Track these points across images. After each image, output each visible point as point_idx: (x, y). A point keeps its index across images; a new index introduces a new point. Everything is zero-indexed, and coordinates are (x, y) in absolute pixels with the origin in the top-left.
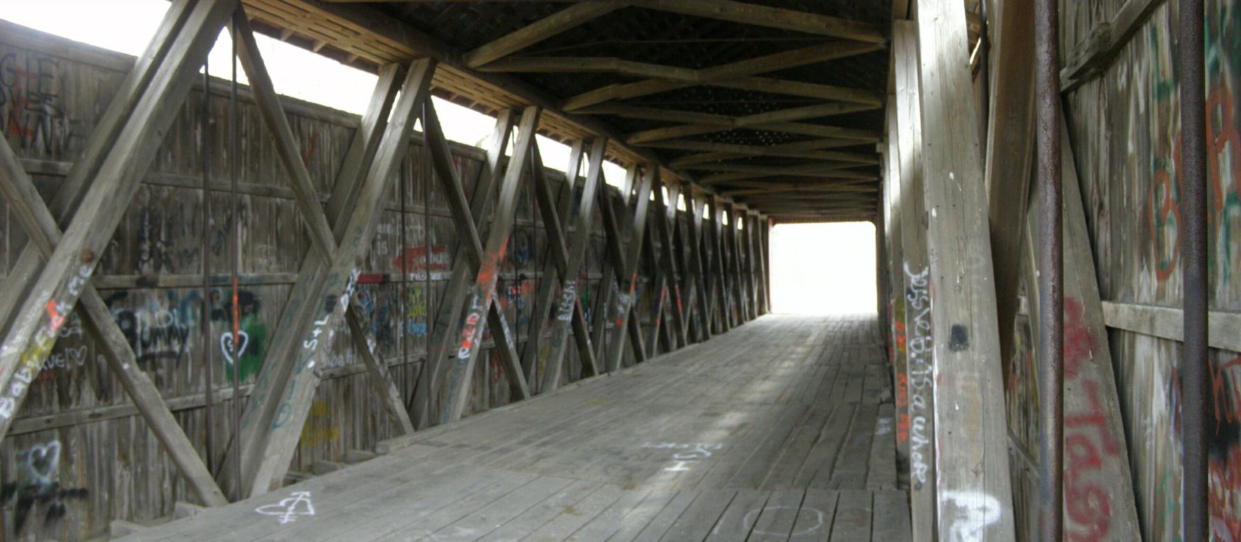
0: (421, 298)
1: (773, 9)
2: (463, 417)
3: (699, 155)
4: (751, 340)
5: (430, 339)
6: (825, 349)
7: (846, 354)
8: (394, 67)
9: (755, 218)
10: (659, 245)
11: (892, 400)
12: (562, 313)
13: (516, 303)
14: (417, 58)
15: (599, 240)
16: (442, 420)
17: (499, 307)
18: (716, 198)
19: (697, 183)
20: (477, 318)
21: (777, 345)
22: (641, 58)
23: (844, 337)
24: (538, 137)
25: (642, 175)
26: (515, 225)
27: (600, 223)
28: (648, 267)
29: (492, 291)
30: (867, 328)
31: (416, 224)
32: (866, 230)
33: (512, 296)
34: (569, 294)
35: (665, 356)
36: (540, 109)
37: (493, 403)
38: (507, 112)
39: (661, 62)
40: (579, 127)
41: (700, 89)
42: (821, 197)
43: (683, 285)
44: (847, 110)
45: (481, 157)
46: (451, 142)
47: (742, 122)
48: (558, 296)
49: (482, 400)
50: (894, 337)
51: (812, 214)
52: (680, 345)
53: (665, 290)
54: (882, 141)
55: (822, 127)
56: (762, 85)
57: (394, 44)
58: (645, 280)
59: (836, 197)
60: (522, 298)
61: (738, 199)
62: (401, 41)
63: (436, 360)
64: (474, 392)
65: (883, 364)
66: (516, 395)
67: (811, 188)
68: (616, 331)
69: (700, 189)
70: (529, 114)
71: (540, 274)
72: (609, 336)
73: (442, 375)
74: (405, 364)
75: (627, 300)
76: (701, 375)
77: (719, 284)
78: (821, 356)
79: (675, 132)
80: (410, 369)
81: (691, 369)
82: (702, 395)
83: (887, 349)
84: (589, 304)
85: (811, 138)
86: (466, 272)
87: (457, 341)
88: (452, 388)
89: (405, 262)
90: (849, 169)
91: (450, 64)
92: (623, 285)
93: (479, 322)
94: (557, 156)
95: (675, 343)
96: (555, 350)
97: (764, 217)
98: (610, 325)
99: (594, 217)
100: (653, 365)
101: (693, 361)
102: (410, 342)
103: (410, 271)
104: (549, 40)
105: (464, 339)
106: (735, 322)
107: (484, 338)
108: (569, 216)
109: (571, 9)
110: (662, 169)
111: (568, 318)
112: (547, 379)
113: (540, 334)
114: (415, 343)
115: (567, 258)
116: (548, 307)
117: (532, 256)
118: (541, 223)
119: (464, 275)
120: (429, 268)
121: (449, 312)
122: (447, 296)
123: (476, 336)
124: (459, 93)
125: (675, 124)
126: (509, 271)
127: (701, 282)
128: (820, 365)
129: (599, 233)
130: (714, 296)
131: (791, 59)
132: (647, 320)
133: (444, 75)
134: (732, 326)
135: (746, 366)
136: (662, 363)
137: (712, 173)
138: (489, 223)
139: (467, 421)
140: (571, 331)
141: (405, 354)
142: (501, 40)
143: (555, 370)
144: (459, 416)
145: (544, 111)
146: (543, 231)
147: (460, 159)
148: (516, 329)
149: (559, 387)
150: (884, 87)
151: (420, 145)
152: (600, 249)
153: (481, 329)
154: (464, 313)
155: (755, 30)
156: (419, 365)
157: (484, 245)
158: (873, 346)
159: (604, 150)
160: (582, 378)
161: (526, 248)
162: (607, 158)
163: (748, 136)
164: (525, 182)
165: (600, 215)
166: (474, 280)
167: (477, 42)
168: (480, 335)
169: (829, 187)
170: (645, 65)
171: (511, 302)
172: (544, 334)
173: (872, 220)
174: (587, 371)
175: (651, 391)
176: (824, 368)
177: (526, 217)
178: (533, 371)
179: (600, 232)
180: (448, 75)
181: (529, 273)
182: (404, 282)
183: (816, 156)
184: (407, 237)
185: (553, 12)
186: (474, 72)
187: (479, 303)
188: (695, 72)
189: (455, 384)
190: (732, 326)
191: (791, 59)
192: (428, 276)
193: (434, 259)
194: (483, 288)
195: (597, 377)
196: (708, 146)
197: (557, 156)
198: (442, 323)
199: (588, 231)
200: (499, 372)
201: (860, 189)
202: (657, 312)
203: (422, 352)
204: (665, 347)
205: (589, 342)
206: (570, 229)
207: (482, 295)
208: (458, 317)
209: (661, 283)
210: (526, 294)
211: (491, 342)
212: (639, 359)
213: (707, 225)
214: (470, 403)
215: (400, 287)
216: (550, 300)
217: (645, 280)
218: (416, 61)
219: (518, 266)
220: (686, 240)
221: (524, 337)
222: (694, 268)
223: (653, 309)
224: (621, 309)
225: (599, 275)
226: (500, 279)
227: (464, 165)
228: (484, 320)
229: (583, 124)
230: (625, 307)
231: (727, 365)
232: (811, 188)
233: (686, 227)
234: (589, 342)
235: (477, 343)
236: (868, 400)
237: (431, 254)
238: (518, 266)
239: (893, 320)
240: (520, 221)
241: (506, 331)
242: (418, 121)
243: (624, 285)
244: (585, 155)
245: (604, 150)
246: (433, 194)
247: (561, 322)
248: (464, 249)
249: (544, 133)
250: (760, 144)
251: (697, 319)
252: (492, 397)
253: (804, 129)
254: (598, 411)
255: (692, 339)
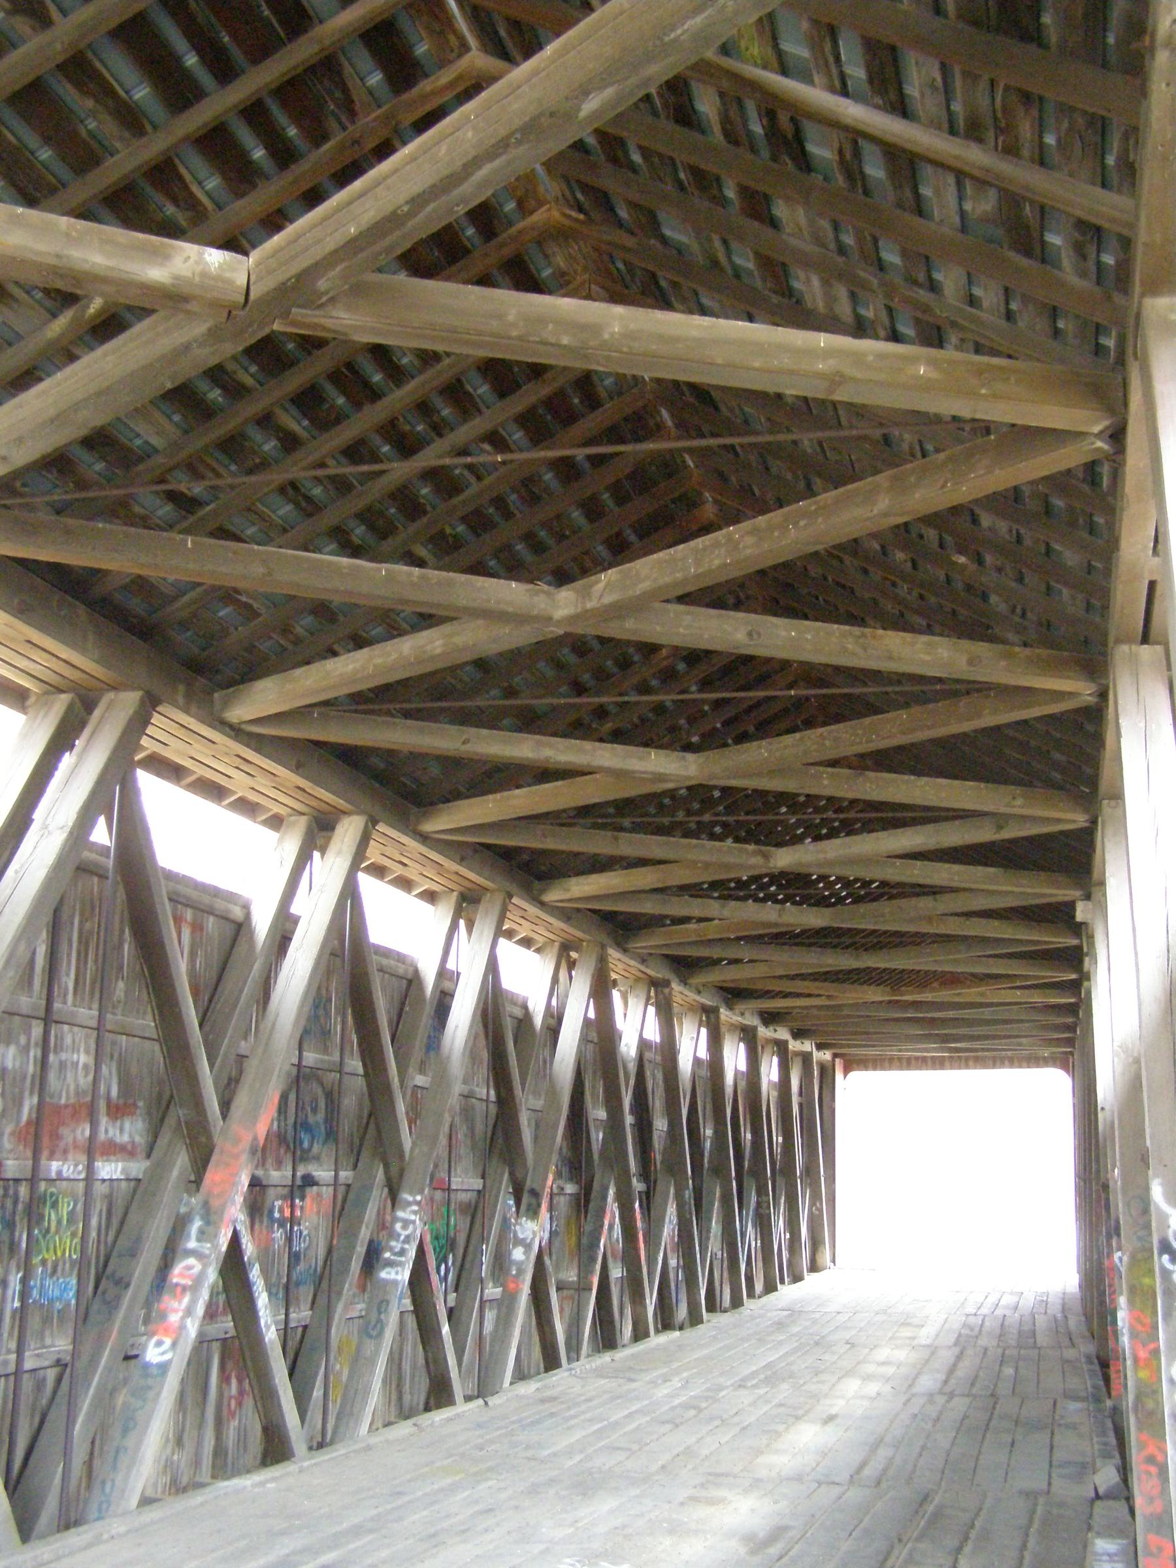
0: (72, 1214)
1: (856, 630)
2: (146, 1502)
3: (692, 926)
4: (795, 1329)
5: (84, 1317)
6: (959, 1357)
7: (1009, 1371)
8: (62, 701)
9: (806, 1058)
10: (602, 1114)
11: (1124, 1492)
12: (390, 1264)
13: (289, 1240)
14: (114, 688)
15: (480, 1107)
16: (93, 1514)
17: (249, 1247)
18: (724, 1014)
19: (684, 982)
20: (196, 1270)
21: (851, 1344)
22: (577, 729)
23: (1002, 1331)
24: (367, 883)
25: (572, 965)
26: (299, 1066)
27: (483, 1071)
28: (577, 1164)
29: (236, 1212)
30: (1055, 1309)
31: (75, 1049)
32: (1047, 1089)
33: (282, 1224)
34: (406, 1223)
35: (607, 1357)
36: (373, 821)
37: (223, 1466)
38: (303, 821)
39: (618, 736)
40: (451, 865)
41: (700, 794)
42: (951, 1014)
43: (648, 1198)
44: (1007, 834)
45: (237, 913)
46: (170, 876)
47: (784, 859)
48: (384, 1226)
49: (197, 1463)
50: (1125, 1340)
51: (933, 1050)
52: (640, 1334)
53: (612, 1207)
54: (1088, 897)
55: (956, 867)
56: (830, 784)
57: (65, 652)
58: (570, 1188)
59: (986, 1014)
60: (305, 1227)
61: (770, 1018)
62: (83, 651)
63: (94, 1361)
64: (179, 1442)
65: (1098, 1400)
66: (275, 1449)
67: (928, 996)
68: (506, 1304)
69: (692, 996)
70: (348, 831)
71: (345, 1175)
72: (490, 1316)
73: (107, 1395)
74: (18, 1372)
75: (533, 1230)
76: (686, 1406)
77: (726, 1200)
78: (951, 1371)
79: (645, 878)
80: (27, 1383)
81: (663, 1391)
82: (688, 1452)
83: (1105, 1364)
84: (452, 1245)
85: (933, 891)
86: (181, 1161)
87: (147, 1321)
88: (126, 1431)
89: (40, 1134)
90: (1010, 956)
91: (187, 711)
92: (526, 1199)
93: (198, 1280)
94: (408, 926)
95: (628, 1330)
96: (369, 1346)
97: (827, 1056)
98: (493, 1291)
99: (471, 1053)
100: (583, 1377)
101: (666, 1371)
102: (34, 1322)
103: (51, 1157)
104: (404, 683)
105: (163, 1316)
106: (759, 1287)
107: (211, 1314)
108: (417, 1053)
109: (446, 628)
110: (613, 954)
111: (402, 1275)
112: (348, 1413)
113: (340, 1308)
114: (47, 1321)
115: (407, 1142)
116: (361, 1250)
117: (331, 1134)
118: (355, 1064)
119: (175, 1173)
120: (93, 1150)
121: (133, 1253)
122: (133, 1217)
123: (189, 1312)
124: (201, 771)
125: (642, 862)
126: (279, 1165)
127: (688, 1194)
128: (951, 1395)
129: (482, 1092)
130: (715, 1227)
131: (893, 729)
132: (571, 1276)
133: (173, 730)
134: (751, 1295)
135: (784, 1391)
136: (599, 1373)
137: (716, 962)
138: (241, 1058)
139: (152, 1514)
140: (407, 1303)
141: (20, 1351)
142: (298, 672)
143: (367, 1392)
144: (134, 1501)
145: (381, 827)
146: (360, 1082)
147: (189, 915)
148: (286, 1295)
149: (372, 1429)
150: (1093, 782)
151: (102, 877)
152: (481, 1127)
153: (205, 1295)
154: (170, 1254)
155: (812, 674)
156: (51, 1375)
157: (226, 1106)
158: (1070, 1354)
159: (502, 919)
160: (427, 1409)
161: (320, 1116)
162: (509, 934)
163: (796, 887)
164: (329, 972)
165: (485, 1055)
166: (198, 1182)
167: (251, 669)
168: (200, 1310)
169: (971, 994)
170: (588, 745)
171: (278, 1234)
172: (349, 1307)
173: (1063, 1063)
174: (439, 1394)
175: (577, 1435)
176: (960, 1405)
177: (326, 1050)
178: (317, 1393)
179: (485, 1091)
180: (181, 733)
181: (323, 1174)
182: (33, 1180)
183: (942, 930)
184: (52, 1076)
185: (415, 628)
186: (236, 732)
187: (202, 1235)
188: (690, 757)
189: (131, 1424)
190: (751, 1295)
191: (893, 729)
192: (90, 1169)
193: (109, 1130)
194: (215, 1203)
195: (462, 1407)
196: (713, 907)
197: (408, 926)
198: (112, 1277)
199: (458, 1088)
200: (241, 1393)
201: (1037, 998)
202: (593, 1260)
203: (60, 1344)
204: (607, 1339)
205: (446, 1329)
206: (420, 1080)
207: (211, 1216)
208: (152, 1270)
209: (604, 1198)
210: (312, 1216)
211: (227, 1325)
212: (551, 1362)
213: (704, 1072)
214: (168, 1466)
215: (23, 1190)
216: (365, 1234)
217: (570, 1188)
218: (111, 695)
219: (300, 1155)
220: (657, 1103)
221: (301, 1314)
222: (673, 1167)
223: (585, 1251)
224: (518, 1254)
225: (478, 1184)
226: (255, 1183)
227: (197, 927)
228: (212, 1275)
229: (462, 860)
230: (528, 1247)
231: (741, 1385)
232: (928, 996)
233: (660, 1076)
234: (446, 1329)
235: (192, 1329)
236: (1063, 1488)
237: (104, 1120)
238: (300, 1155)
239: (1122, 1301)
240: (311, 1058)
241: (262, 1300)
242: (102, 820)
243: (525, 1197)
244: (462, 922)
245: (502, 919)
246: (121, 985)
247: (387, 1282)
248: (180, 1112)
249: (378, 871)
250: (821, 902)
251: (677, 1275)
252: (219, 1451)
253: (919, 872)
254: (453, 1489)
255: (666, 1323)
